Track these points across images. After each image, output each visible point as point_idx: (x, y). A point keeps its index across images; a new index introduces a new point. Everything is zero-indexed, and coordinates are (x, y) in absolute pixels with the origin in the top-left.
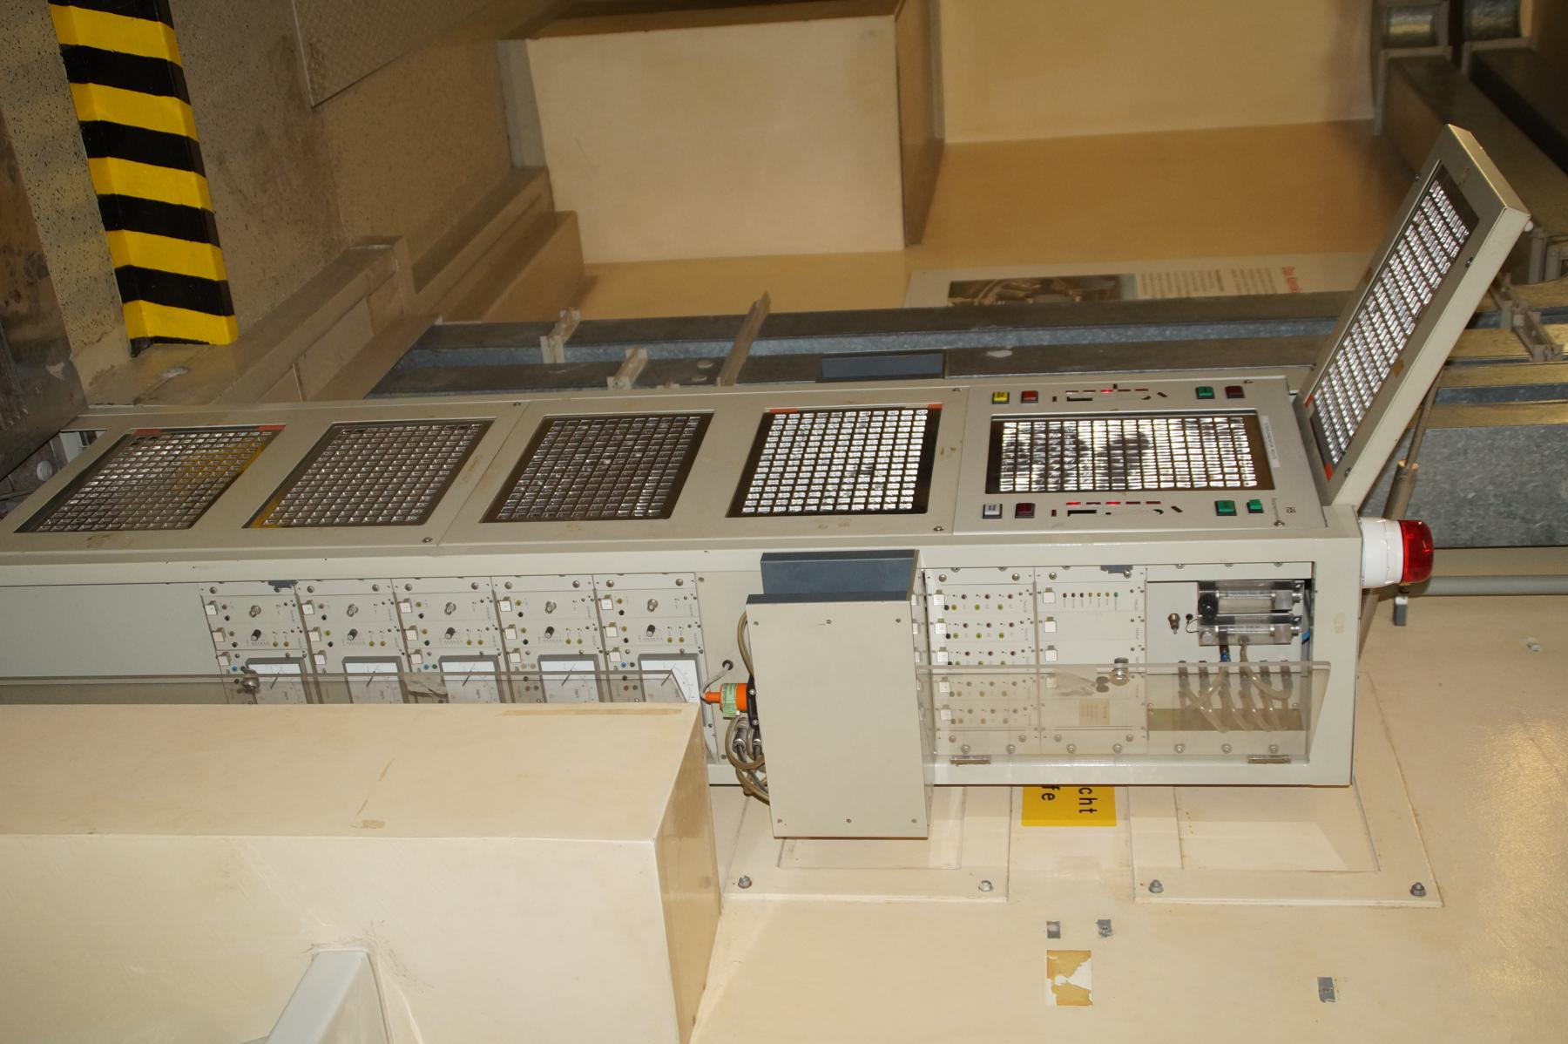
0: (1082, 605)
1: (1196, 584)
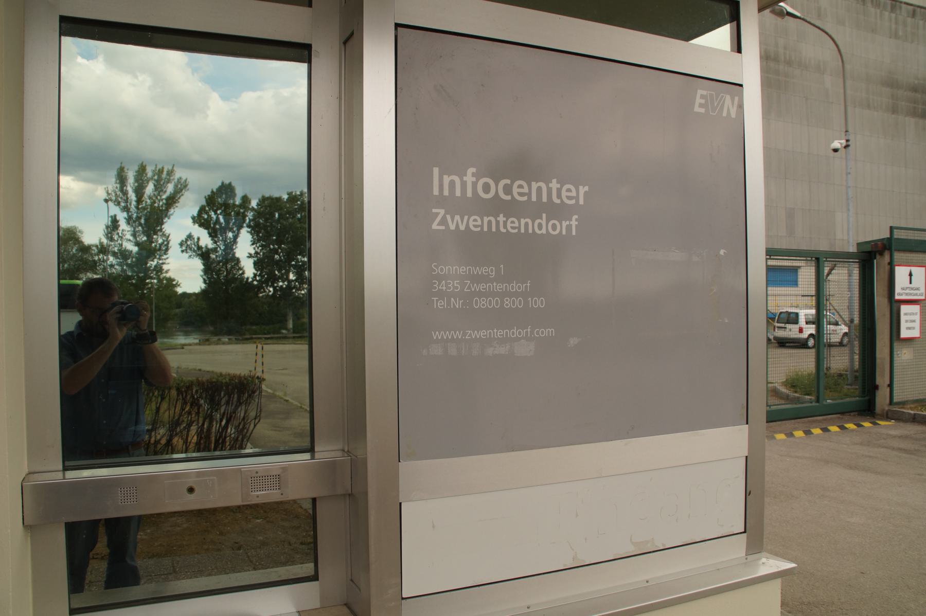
0: (911, 283)
1: (62, 315)
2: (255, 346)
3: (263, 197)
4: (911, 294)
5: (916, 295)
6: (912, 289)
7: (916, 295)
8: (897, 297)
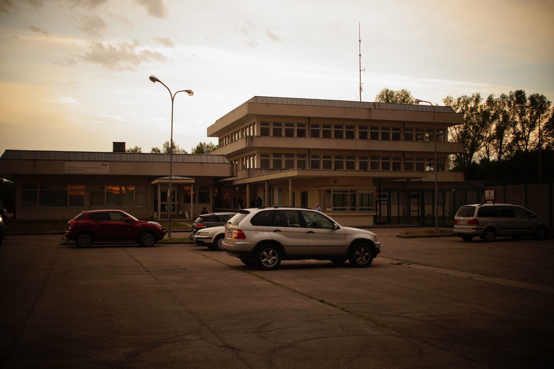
0: (489, 195)
1: (308, 207)
2: (422, 181)
3: (136, 149)
4: (490, 198)
5: (491, 198)
6: (490, 196)
7: (491, 198)
8: (486, 199)
